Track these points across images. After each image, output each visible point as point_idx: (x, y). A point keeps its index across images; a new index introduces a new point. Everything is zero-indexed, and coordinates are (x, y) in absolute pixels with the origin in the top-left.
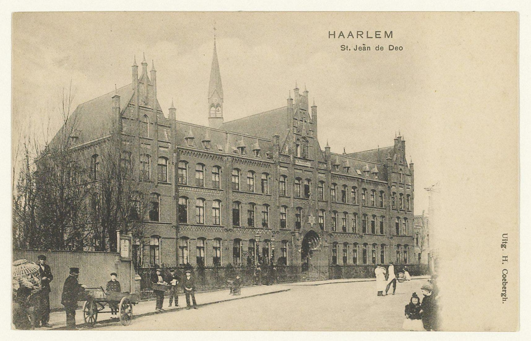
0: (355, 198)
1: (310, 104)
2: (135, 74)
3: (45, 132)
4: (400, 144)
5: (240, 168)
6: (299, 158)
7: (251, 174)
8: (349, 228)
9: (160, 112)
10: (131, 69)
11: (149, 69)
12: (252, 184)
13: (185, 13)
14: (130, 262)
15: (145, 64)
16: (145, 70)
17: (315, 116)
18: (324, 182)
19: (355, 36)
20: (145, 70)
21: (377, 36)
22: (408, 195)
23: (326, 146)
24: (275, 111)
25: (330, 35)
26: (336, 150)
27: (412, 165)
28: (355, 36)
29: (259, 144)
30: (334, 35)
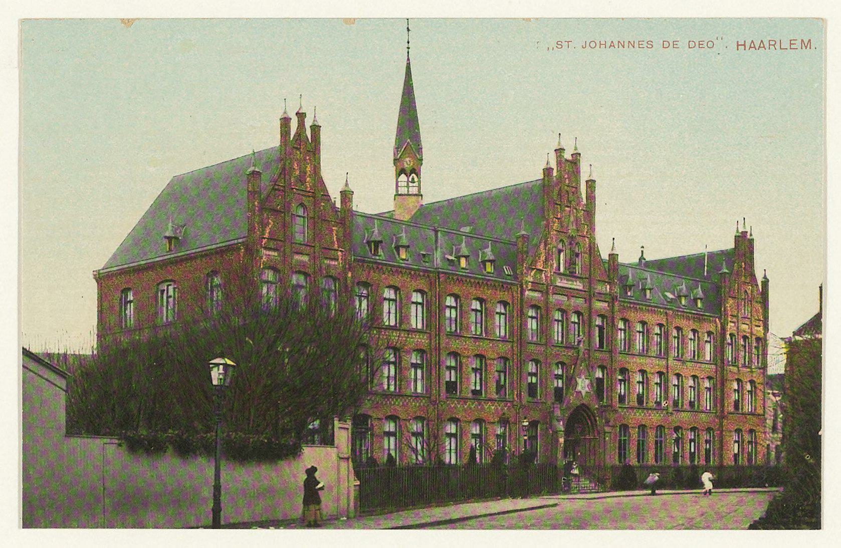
0: (660, 343)
1: (584, 177)
2: (285, 133)
3: (108, 230)
4: (744, 245)
5: (485, 297)
6: (563, 275)
7: (392, 292)
8: (682, 402)
10: (278, 124)
11: (308, 123)
12: (453, 316)
13: (249, 22)
14: (348, 459)
15: (301, 116)
16: (301, 124)
17: (591, 197)
18: (606, 317)
19: (767, 46)
20: (301, 124)
21: (792, 46)
22: (758, 339)
23: (609, 252)
24: (504, 190)
25: (738, 45)
26: (628, 257)
27: (766, 283)
28: (767, 46)
29: (492, 250)
30: (744, 45)
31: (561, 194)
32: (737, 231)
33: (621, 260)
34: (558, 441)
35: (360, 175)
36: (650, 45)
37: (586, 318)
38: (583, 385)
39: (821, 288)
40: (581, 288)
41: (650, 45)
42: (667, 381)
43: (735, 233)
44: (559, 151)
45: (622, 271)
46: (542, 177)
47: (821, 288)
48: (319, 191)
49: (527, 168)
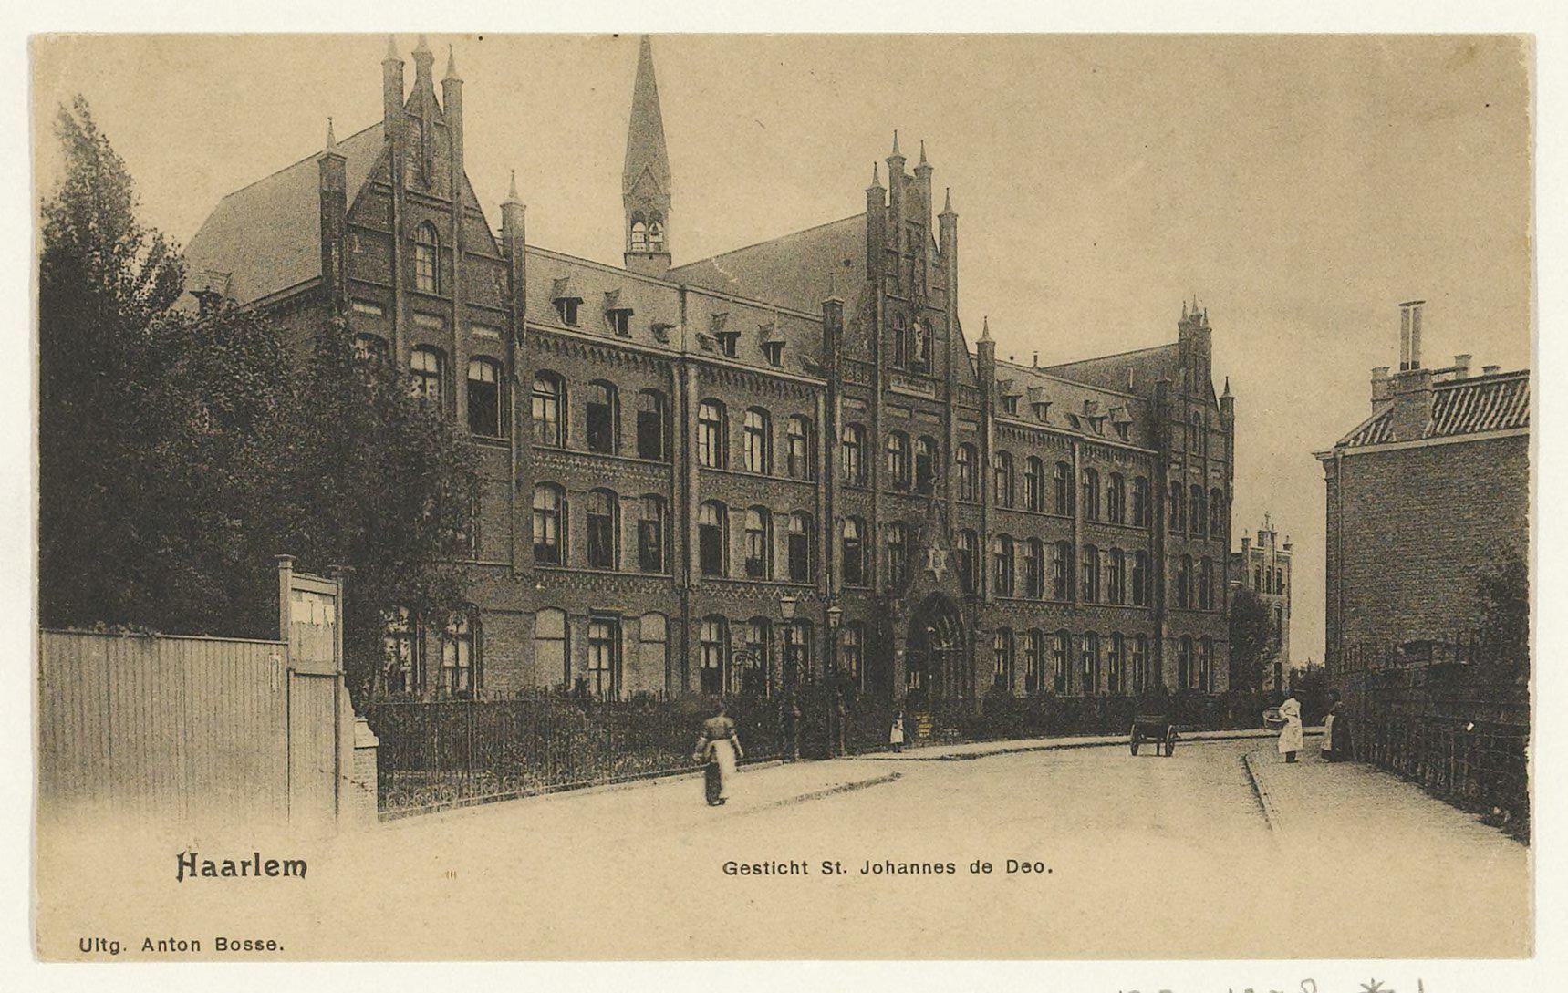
1: (937, 208)
9: (477, 213)
22: (1215, 492)
31: (900, 249)
32: (1184, 316)
33: (1000, 354)
34: (894, 651)
35: (554, 200)
36: (952, 868)
37: (940, 447)
38: (937, 560)
39: (272, 945)
40: (932, 397)
41: (952, 868)
42: (1072, 557)
43: (1179, 318)
44: (896, 161)
45: (1000, 374)
46: (865, 209)
47: (272, 945)
48: (463, 208)
49: (844, 205)
